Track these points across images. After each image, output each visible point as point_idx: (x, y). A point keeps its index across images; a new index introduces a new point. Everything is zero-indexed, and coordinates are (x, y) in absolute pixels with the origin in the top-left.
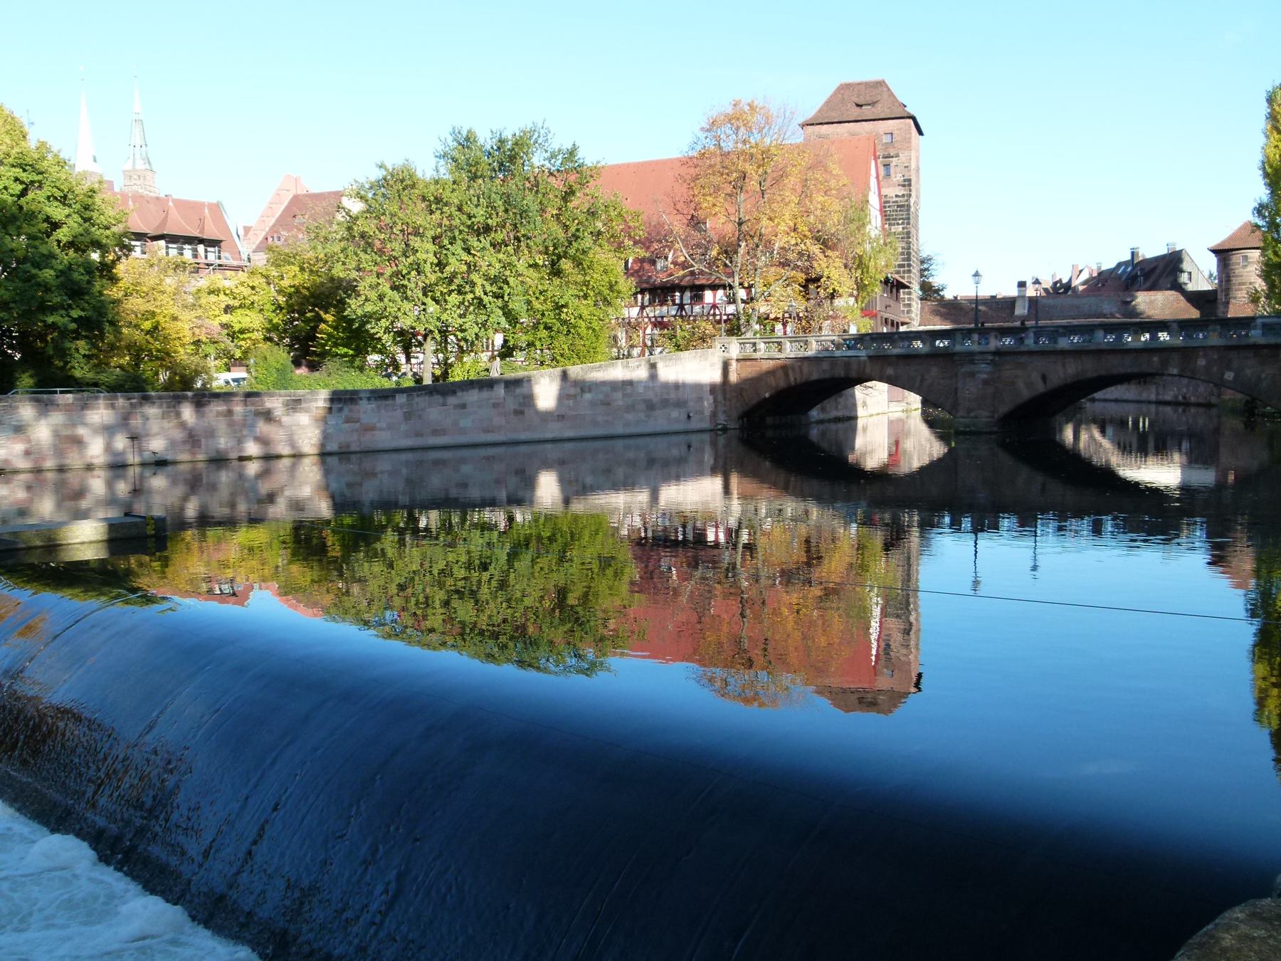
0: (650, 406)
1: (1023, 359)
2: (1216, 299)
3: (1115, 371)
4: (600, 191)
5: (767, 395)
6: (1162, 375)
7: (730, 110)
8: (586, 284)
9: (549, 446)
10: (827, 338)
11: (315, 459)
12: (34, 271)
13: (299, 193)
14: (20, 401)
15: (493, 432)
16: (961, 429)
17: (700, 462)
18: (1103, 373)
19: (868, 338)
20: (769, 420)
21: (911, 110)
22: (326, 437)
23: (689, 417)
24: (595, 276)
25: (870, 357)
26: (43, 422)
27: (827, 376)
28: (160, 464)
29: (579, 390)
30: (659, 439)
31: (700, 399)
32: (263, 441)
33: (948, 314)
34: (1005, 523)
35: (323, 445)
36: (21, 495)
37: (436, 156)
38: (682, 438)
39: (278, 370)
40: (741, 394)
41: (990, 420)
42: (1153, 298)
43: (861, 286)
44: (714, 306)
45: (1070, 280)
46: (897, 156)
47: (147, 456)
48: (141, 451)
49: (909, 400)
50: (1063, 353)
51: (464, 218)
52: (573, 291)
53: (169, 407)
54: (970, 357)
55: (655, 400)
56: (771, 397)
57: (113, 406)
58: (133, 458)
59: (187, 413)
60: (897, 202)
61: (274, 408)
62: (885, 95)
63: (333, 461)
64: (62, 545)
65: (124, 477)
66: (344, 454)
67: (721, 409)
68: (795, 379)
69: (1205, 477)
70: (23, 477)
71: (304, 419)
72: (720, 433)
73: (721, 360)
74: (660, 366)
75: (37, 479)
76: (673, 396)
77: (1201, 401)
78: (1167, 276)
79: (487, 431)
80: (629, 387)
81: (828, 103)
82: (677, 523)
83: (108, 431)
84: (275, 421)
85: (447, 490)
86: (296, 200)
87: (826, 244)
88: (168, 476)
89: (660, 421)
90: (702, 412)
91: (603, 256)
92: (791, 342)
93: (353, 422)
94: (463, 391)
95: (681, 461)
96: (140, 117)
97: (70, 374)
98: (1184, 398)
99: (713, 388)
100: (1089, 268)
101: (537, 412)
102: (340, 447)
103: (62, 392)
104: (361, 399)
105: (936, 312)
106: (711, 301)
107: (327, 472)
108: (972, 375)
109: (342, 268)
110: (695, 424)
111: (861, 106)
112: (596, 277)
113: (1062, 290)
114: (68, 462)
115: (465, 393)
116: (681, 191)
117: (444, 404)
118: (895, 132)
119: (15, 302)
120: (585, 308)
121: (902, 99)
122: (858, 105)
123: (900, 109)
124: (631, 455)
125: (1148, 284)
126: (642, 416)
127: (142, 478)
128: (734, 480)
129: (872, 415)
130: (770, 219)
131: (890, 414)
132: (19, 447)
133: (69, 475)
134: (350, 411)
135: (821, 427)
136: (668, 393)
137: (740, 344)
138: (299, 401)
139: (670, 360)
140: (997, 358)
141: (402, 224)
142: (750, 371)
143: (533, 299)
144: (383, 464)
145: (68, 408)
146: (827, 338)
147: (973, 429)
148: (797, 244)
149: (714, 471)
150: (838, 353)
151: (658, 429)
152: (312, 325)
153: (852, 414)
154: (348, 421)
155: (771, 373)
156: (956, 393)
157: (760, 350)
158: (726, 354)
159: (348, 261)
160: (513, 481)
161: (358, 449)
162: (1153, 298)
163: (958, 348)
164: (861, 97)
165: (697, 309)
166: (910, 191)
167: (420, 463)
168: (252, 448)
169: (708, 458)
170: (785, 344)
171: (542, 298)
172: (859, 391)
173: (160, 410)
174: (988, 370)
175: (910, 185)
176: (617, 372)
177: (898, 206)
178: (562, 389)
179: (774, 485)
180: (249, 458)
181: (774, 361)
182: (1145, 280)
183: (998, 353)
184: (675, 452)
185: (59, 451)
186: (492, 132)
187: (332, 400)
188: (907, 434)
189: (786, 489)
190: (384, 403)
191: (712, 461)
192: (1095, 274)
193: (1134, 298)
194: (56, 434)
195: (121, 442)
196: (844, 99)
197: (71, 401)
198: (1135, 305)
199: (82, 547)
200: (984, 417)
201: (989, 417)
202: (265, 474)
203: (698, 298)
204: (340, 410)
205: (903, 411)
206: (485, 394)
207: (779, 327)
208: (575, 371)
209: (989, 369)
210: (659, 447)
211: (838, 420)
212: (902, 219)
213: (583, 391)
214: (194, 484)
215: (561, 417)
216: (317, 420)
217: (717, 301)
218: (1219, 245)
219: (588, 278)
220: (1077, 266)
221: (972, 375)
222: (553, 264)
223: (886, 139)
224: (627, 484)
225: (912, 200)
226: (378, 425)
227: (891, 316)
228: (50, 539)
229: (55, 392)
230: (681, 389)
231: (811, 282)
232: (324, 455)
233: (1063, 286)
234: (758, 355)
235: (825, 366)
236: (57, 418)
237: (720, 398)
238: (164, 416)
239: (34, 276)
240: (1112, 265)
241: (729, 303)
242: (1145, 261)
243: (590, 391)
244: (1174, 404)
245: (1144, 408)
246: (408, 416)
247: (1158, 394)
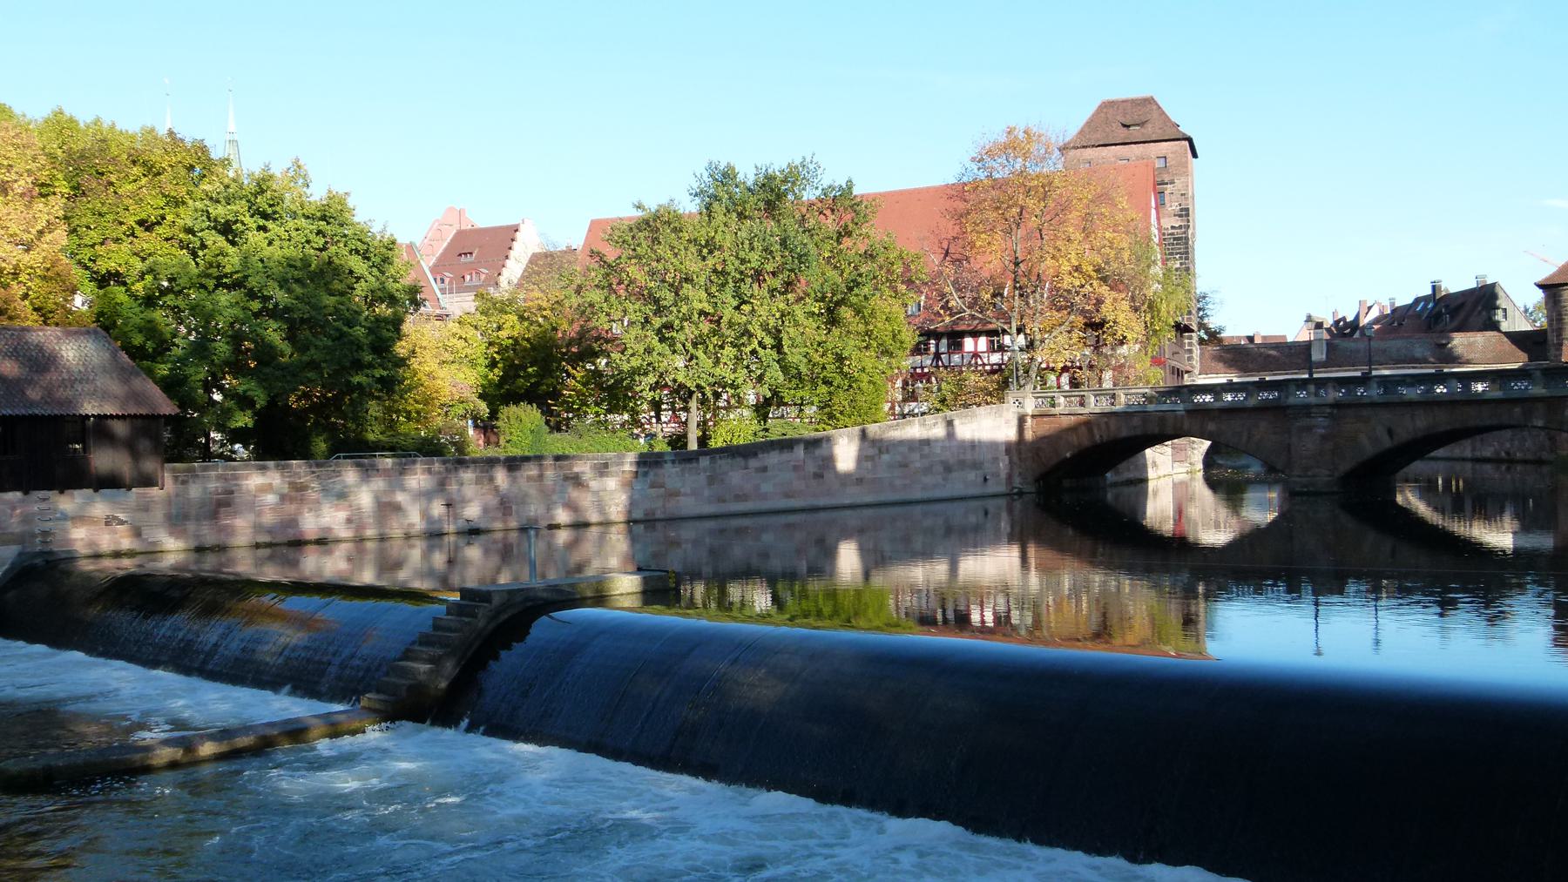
0: (948, 469)
1: (1365, 412)
2: (1545, 341)
4: (874, 232)
5: (1068, 455)
6: (1526, 426)
7: (1003, 139)
8: (868, 333)
9: (848, 512)
12: (345, 329)
16: (1297, 489)
17: (997, 530)
19: (1185, 390)
20: (1067, 483)
21: (1185, 129)
22: (632, 504)
23: (985, 480)
24: (879, 325)
25: (1188, 411)
26: (364, 488)
27: (1139, 432)
28: (472, 532)
30: (956, 504)
31: (996, 460)
32: (572, 506)
34: (1351, 588)
35: (630, 512)
37: (691, 194)
39: (532, 432)
40: (1038, 455)
42: (1472, 339)
43: (1151, 332)
44: (976, 355)
45: (1357, 317)
46: (1172, 182)
48: (456, 517)
49: (1192, 460)
50: (1411, 404)
51: (737, 263)
52: (852, 342)
53: (482, 472)
54: (1306, 409)
55: (952, 461)
56: (1074, 457)
57: (429, 471)
59: (501, 476)
60: (1172, 234)
61: (582, 473)
62: (1155, 115)
65: (440, 547)
66: (649, 522)
67: (1016, 472)
69: (1544, 541)
71: (612, 483)
72: (1016, 497)
74: (956, 423)
75: (357, 548)
76: (969, 457)
77: (1529, 457)
79: (787, 496)
80: (926, 447)
81: (1089, 123)
82: (934, 603)
84: (583, 486)
86: (461, 234)
87: (1115, 282)
89: (963, 483)
91: (884, 304)
92: (1095, 396)
95: (977, 529)
96: (236, 137)
98: (1508, 453)
99: (1009, 448)
100: (1379, 304)
101: (837, 474)
102: (646, 515)
103: (345, 458)
104: (666, 462)
106: (972, 349)
107: (633, 538)
108: (1309, 429)
109: (607, 318)
110: (992, 488)
112: (880, 327)
115: (765, 455)
117: (746, 468)
118: (1170, 156)
119: (325, 361)
120: (869, 360)
121: (1174, 119)
122: (1124, 126)
123: (1174, 130)
124: (928, 522)
126: (939, 479)
127: (457, 548)
128: (1032, 551)
130: (1053, 257)
131: (1174, 476)
132: (342, 515)
134: (656, 475)
136: (964, 453)
138: (606, 465)
139: (966, 416)
140: (1335, 411)
142: (1047, 427)
144: (688, 532)
145: (386, 473)
146: (1139, 391)
147: (1311, 489)
149: (1011, 539)
150: (1151, 408)
153: (1138, 475)
154: (652, 486)
155: (1073, 429)
156: (1289, 451)
157: (1059, 405)
158: (1020, 410)
159: (612, 311)
160: (813, 552)
161: (662, 516)
162: (1472, 339)
164: (1128, 116)
165: (956, 358)
166: (1188, 221)
168: (562, 516)
169: (1004, 525)
171: (821, 350)
172: (1148, 452)
174: (1326, 424)
175: (1188, 215)
176: (914, 430)
177: (1174, 239)
178: (860, 450)
179: (1078, 554)
180: (558, 527)
181: (1076, 417)
183: (1337, 405)
184: (973, 519)
187: (638, 464)
188: (1191, 499)
189: (1093, 560)
190: (688, 466)
191: (1009, 529)
192: (1388, 311)
193: (1450, 340)
195: (438, 509)
196: (1107, 118)
197: (390, 466)
199: (621, 599)
200: (1323, 477)
201: (1329, 476)
204: (646, 474)
205: (1187, 473)
206: (786, 456)
209: (1326, 422)
210: (957, 512)
213: (880, 452)
214: (506, 554)
215: (860, 481)
218: (1547, 279)
219: (871, 327)
222: (829, 311)
223: (1160, 164)
224: (927, 554)
225: (1190, 232)
226: (682, 490)
227: (1178, 365)
228: (597, 591)
229: (375, 456)
230: (977, 449)
231: (1095, 326)
232: (631, 522)
233: (1347, 325)
234: (1057, 410)
235: (1136, 421)
236: (379, 484)
237: (1015, 459)
238: (478, 482)
240: (1410, 301)
242: (1449, 296)
243: (888, 451)
244: (1495, 461)
245: (1458, 466)
246: (711, 480)
247: (1474, 450)
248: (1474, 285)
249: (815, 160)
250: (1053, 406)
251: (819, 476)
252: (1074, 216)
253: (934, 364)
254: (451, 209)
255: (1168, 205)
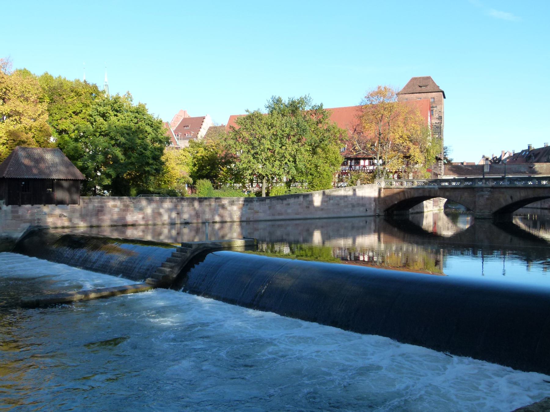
0: (353, 206)
1: (502, 190)
3: (541, 195)
4: (330, 122)
7: (376, 90)
8: (326, 158)
9: (318, 220)
10: (422, 180)
11: (238, 223)
12: (144, 151)
13: (185, 117)
14: (142, 199)
15: (298, 214)
17: (370, 229)
18: (536, 196)
20: (395, 212)
21: (441, 88)
22: (242, 215)
23: (366, 210)
24: (331, 155)
25: (439, 188)
26: (149, 207)
27: (421, 195)
28: (186, 223)
29: (328, 199)
30: (356, 219)
31: (370, 204)
33: (455, 171)
35: (241, 218)
36: (141, 234)
37: (266, 107)
38: (364, 219)
39: (208, 189)
41: (490, 214)
43: (427, 160)
44: (364, 166)
45: (501, 156)
46: (436, 107)
47: (182, 221)
48: (181, 218)
51: (281, 132)
54: (481, 189)
56: (398, 203)
57: (172, 202)
58: (178, 221)
60: (436, 125)
62: (431, 83)
63: (244, 224)
64: (232, 247)
66: (248, 222)
67: (378, 207)
68: (408, 196)
70: (142, 227)
71: (235, 208)
72: (377, 217)
73: (378, 188)
74: (357, 190)
76: (361, 202)
78: (545, 156)
79: (296, 214)
80: (346, 198)
83: (170, 210)
84: (225, 208)
85: (282, 237)
86: (185, 120)
87: (414, 142)
88: (189, 228)
89: (347, 212)
90: (371, 209)
93: (251, 209)
94: (289, 198)
95: (363, 227)
97: (148, 189)
99: (375, 199)
100: (509, 152)
101: (314, 207)
102: (246, 219)
103: (142, 196)
104: (254, 201)
105: (451, 170)
106: (363, 164)
108: (482, 196)
110: (369, 213)
111: (421, 87)
112: (331, 155)
113: (497, 161)
114: (156, 222)
115: (289, 199)
116: (356, 121)
118: (435, 98)
125: (536, 160)
126: (350, 209)
127: (180, 229)
128: (382, 236)
129: (428, 211)
132: (141, 216)
133: (156, 227)
135: (412, 215)
137: (385, 182)
140: (492, 190)
141: (259, 134)
142: (389, 193)
143: (306, 164)
144: (261, 226)
146: (422, 180)
147: (482, 217)
148: (403, 143)
149: (375, 232)
150: (426, 187)
151: (356, 215)
152: (208, 171)
153: (418, 210)
154: (250, 209)
155: (398, 193)
157: (393, 185)
158: (380, 186)
161: (253, 220)
162: (542, 166)
163: (476, 185)
165: (357, 167)
166: (441, 121)
167: (273, 226)
168: (217, 219)
169: (373, 226)
170: (404, 182)
172: (425, 202)
173: (187, 204)
174: (489, 194)
175: (441, 119)
177: (436, 127)
178: (323, 199)
180: (215, 222)
182: (535, 158)
183: (492, 187)
184: (362, 224)
185: (154, 218)
186: (289, 98)
188: (440, 219)
189: (404, 240)
190: (262, 202)
191: (374, 228)
193: (534, 165)
194: (153, 211)
195: (174, 215)
198: (535, 168)
200: (487, 213)
201: (489, 212)
202: (222, 228)
203: (357, 163)
204: (247, 205)
205: (438, 210)
206: (296, 200)
207: (391, 175)
208: (327, 191)
209: (489, 193)
211: (418, 213)
212: (438, 132)
213: (330, 199)
214: (197, 231)
216: (239, 209)
217: (366, 164)
220: (504, 151)
221: (482, 196)
225: (442, 125)
226: (260, 211)
229: (153, 196)
230: (364, 199)
231: (407, 157)
232: (241, 222)
233: (497, 159)
234: (393, 187)
235: (420, 191)
236: (154, 205)
237: (377, 203)
238: (188, 206)
239: (143, 153)
240: (520, 151)
241: (371, 165)
242: (534, 150)
243: (332, 200)
245: (535, 210)
246: (270, 208)
247: (541, 204)
248: (544, 146)
249: (309, 96)
250: (391, 185)
251: (308, 207)
252: (401, 118)
253: (350, 169)
254: (181, 110)
255: (434, 115)
